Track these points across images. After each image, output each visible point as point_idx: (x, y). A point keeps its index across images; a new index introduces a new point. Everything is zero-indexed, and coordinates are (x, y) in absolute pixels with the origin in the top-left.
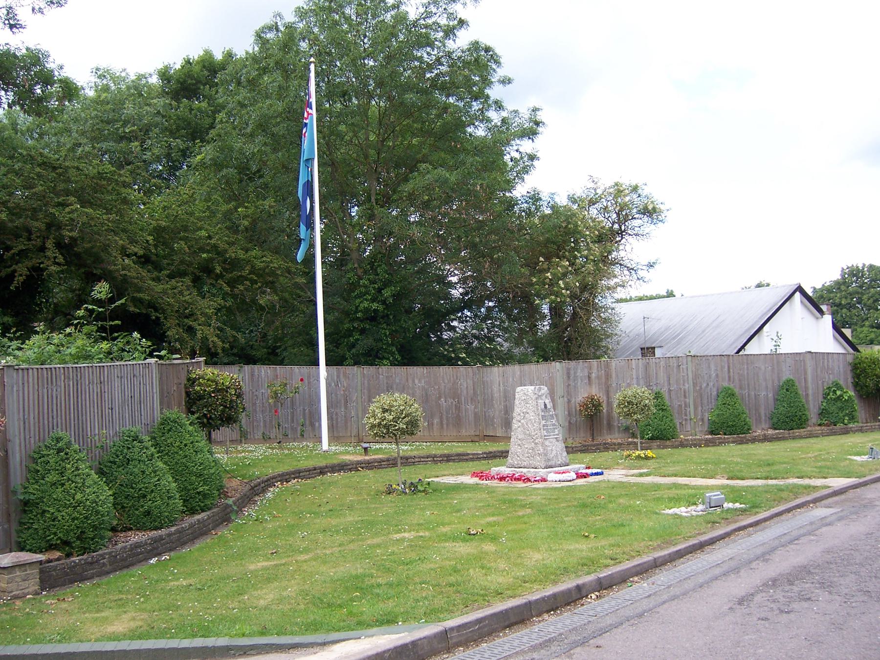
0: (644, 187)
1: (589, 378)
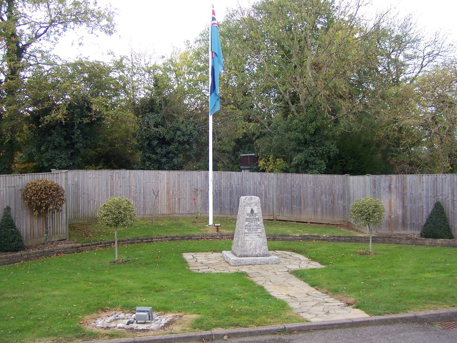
0: (100, 9)
1: (390, 187)
